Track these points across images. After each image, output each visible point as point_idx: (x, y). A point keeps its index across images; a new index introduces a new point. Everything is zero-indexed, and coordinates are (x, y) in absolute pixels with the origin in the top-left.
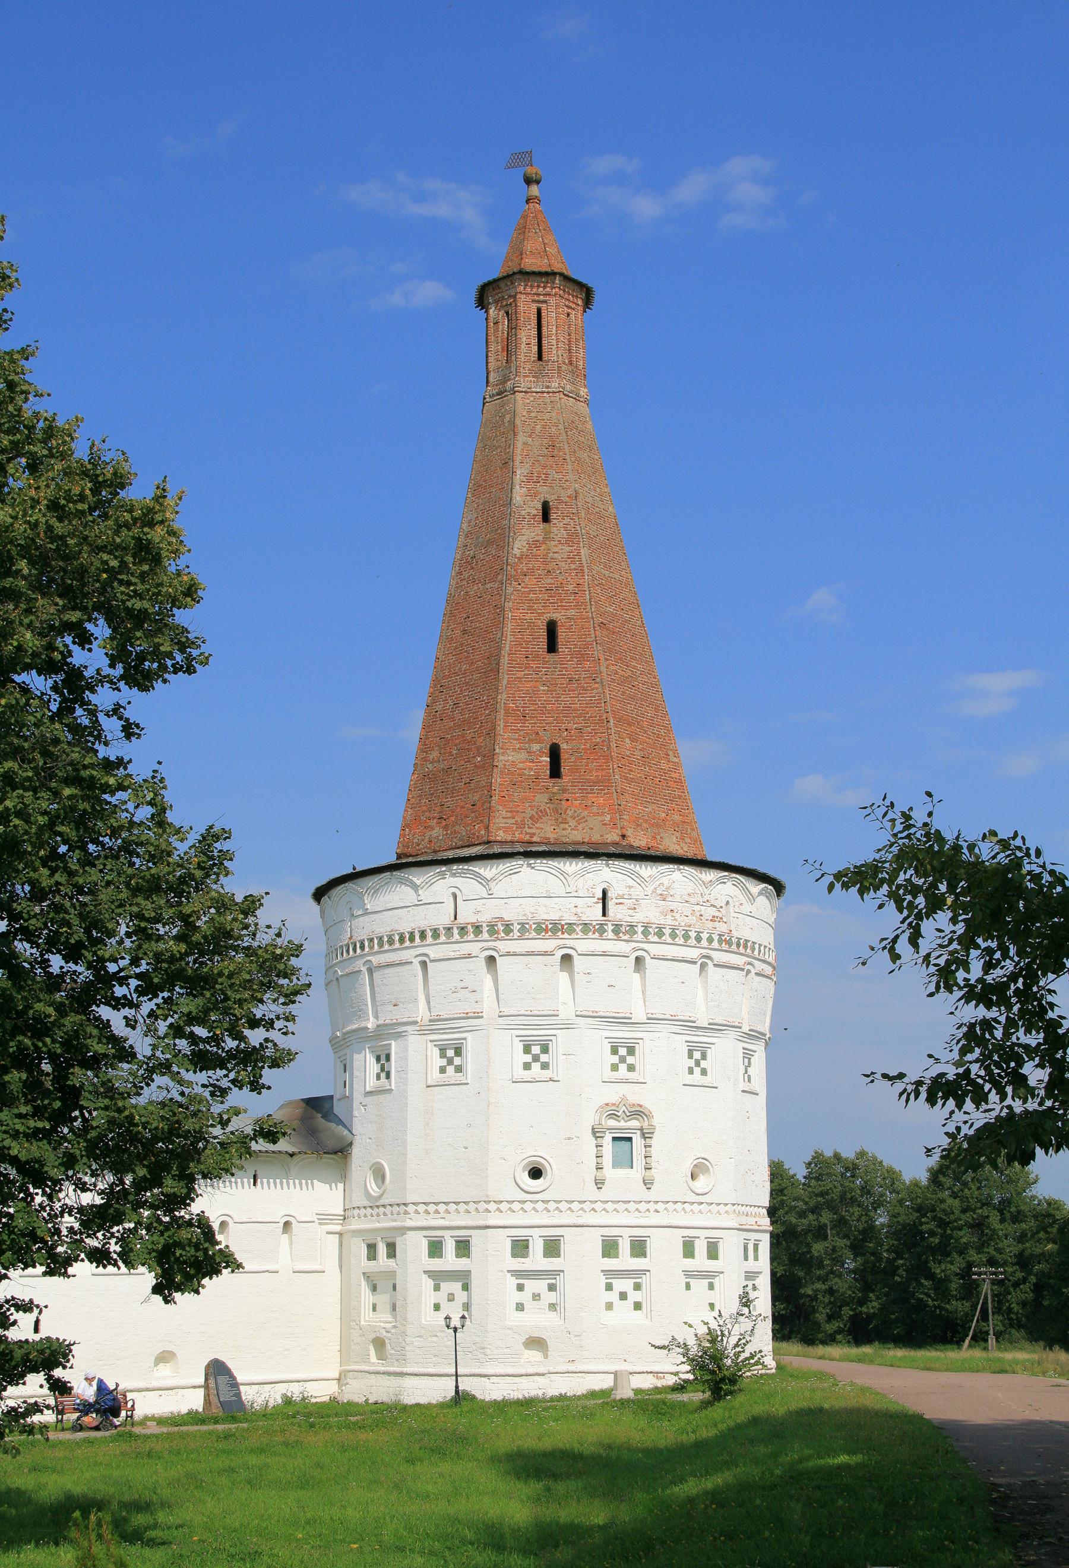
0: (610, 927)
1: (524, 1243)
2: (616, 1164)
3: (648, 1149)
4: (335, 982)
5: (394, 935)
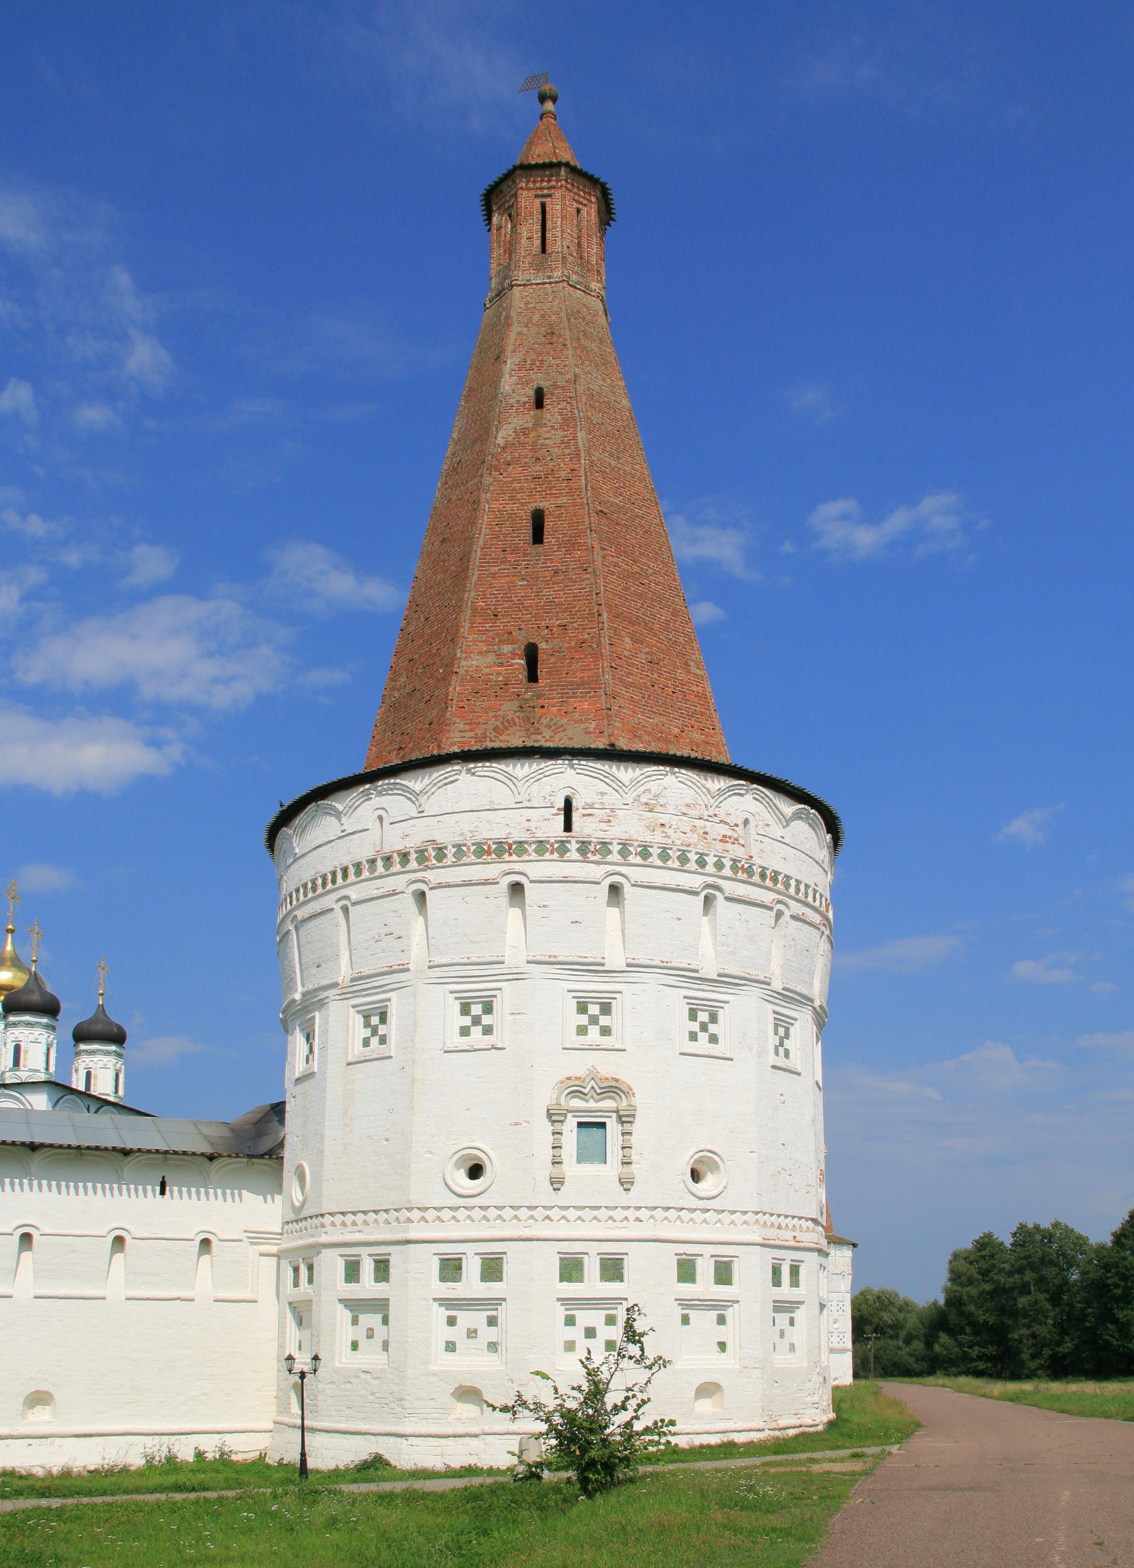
0: (573, 846)
1: (456, 1263)
2: (583, 1157)
3: (626, 1137)
5: (316, 879)
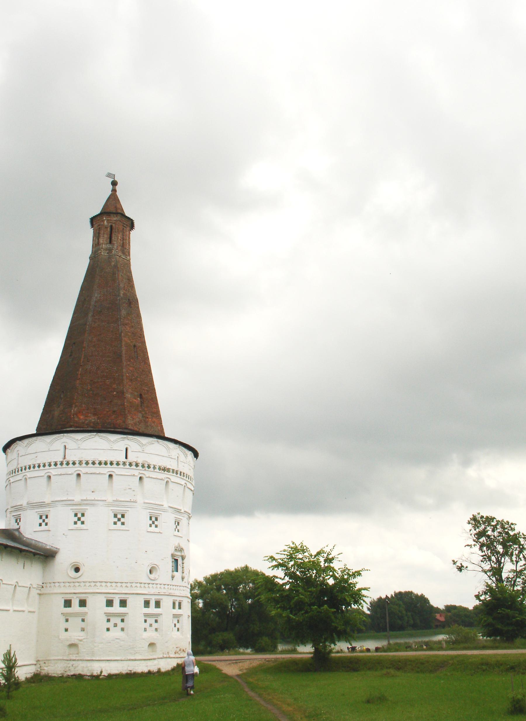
4: (23, 482)
